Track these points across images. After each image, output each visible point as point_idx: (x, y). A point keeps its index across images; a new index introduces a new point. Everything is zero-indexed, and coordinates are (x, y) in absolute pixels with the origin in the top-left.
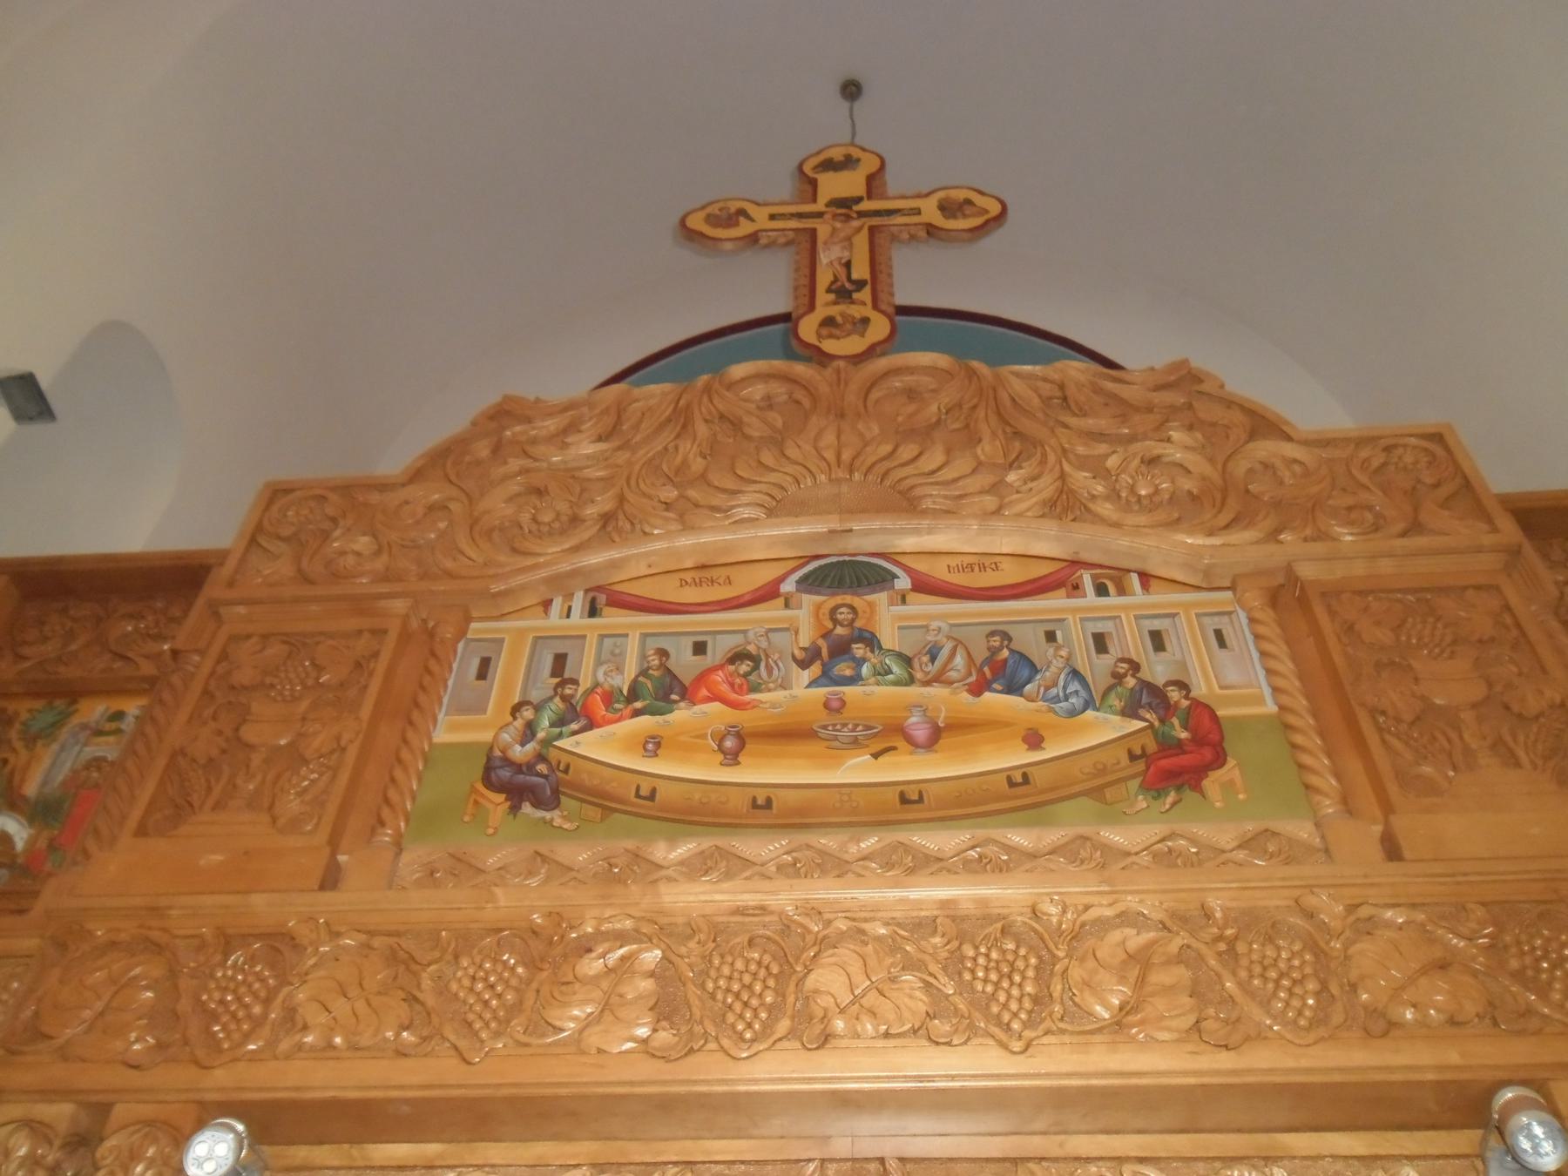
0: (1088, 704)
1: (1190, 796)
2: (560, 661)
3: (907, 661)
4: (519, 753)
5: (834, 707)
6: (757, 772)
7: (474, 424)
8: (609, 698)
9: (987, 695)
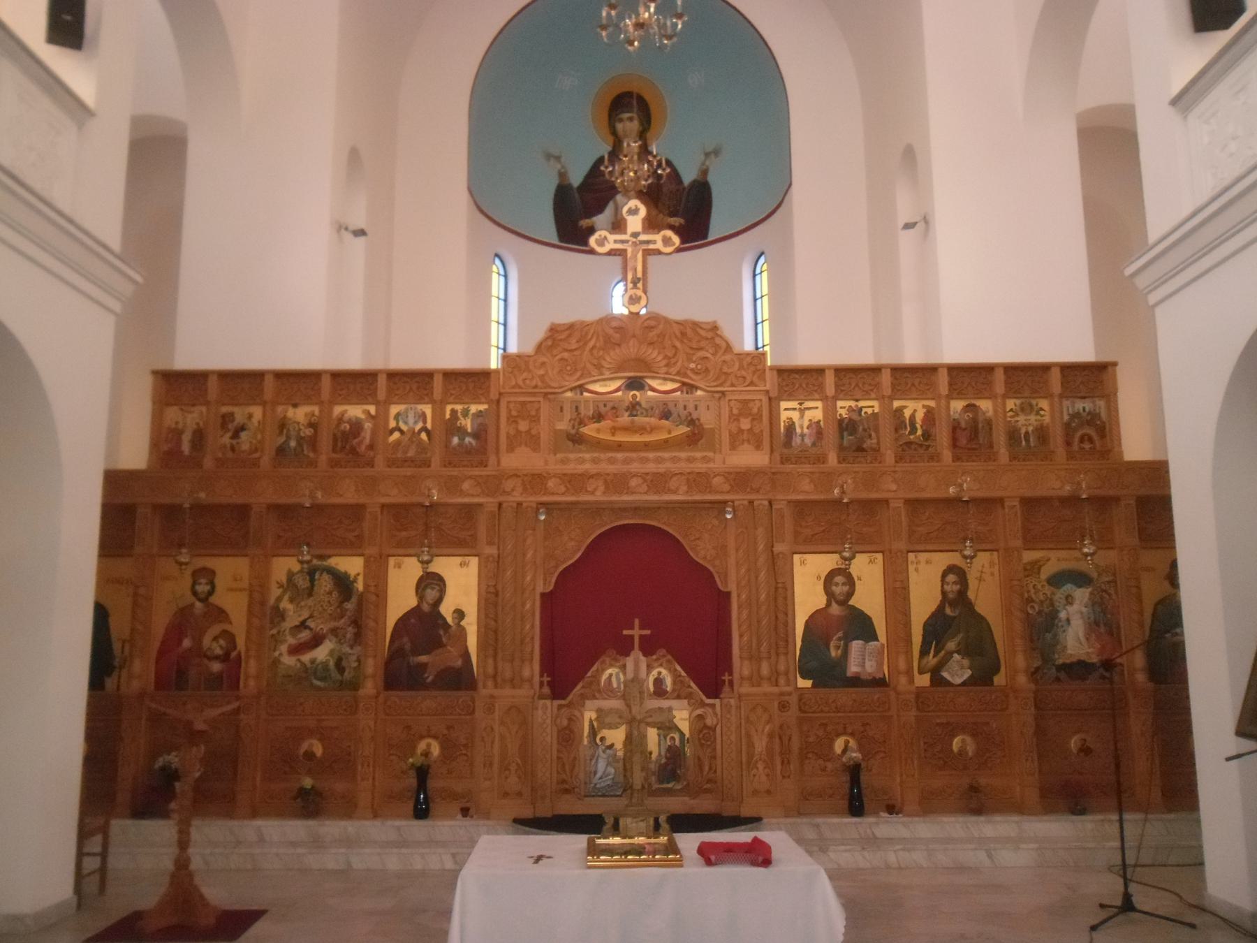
0: (680, 424)
2: (577, 407)
4: (573, 432)
5: (633, 422)
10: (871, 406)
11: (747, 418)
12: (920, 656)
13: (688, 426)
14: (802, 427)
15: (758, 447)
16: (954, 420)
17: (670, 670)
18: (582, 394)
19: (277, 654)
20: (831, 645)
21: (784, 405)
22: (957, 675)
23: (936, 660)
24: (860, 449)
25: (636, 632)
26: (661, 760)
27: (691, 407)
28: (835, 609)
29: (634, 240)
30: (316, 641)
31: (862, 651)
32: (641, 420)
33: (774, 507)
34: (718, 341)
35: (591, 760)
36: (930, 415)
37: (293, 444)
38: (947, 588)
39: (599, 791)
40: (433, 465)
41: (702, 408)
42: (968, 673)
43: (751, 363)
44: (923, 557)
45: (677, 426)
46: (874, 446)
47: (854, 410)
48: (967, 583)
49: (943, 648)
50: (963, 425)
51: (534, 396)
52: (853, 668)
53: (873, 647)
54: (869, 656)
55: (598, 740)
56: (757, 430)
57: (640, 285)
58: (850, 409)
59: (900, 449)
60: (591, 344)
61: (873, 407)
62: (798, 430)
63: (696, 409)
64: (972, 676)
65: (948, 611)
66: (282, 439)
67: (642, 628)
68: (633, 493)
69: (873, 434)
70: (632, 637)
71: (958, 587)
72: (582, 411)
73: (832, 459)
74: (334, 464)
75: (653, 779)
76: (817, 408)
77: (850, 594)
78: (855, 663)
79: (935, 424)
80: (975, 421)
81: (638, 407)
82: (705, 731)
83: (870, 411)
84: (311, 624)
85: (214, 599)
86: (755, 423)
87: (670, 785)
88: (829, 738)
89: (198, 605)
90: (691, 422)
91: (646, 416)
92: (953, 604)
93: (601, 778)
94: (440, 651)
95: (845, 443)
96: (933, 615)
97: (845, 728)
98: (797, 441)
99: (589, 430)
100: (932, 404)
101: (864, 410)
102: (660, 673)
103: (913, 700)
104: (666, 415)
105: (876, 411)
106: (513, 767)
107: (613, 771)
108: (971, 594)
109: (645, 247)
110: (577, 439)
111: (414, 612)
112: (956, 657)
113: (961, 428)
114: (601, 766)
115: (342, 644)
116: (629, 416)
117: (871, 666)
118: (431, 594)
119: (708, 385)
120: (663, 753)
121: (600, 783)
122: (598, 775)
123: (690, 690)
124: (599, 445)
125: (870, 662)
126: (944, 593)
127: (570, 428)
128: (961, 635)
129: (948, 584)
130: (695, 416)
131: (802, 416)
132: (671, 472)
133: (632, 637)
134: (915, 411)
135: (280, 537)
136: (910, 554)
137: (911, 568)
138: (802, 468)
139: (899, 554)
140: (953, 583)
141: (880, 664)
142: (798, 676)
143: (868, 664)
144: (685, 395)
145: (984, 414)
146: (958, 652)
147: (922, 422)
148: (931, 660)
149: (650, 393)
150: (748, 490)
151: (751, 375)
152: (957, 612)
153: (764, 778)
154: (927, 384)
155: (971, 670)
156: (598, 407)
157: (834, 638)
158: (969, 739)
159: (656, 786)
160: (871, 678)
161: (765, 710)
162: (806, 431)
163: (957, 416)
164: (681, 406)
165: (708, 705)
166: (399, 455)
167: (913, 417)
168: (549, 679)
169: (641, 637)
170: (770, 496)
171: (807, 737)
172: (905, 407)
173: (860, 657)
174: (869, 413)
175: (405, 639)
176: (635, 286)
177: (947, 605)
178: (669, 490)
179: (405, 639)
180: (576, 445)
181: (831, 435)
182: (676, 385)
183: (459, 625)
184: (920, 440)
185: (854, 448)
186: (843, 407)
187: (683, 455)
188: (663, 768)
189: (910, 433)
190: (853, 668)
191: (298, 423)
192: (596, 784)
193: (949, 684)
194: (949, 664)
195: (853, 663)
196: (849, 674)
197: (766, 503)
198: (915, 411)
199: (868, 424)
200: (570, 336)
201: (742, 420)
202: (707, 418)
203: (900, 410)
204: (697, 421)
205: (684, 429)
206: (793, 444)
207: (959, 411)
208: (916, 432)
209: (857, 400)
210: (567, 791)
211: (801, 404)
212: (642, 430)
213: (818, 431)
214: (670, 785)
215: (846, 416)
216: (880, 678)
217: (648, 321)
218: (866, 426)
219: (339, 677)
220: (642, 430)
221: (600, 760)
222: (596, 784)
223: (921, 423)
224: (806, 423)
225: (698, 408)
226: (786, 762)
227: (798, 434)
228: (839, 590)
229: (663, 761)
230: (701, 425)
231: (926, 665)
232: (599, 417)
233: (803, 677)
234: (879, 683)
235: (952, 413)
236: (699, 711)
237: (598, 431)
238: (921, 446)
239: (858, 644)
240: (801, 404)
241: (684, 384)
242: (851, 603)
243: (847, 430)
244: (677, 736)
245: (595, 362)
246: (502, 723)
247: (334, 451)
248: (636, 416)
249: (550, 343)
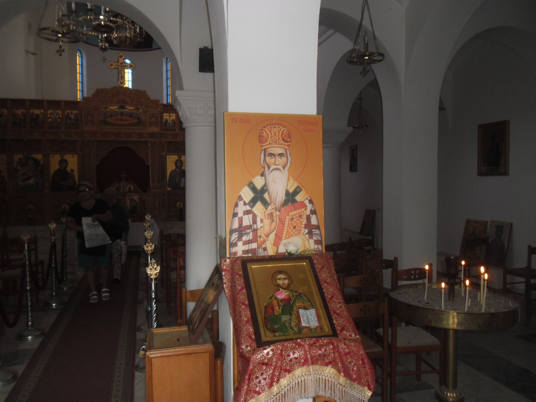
6: (118, 122)
28: (178, 170)
62: (168, 122)
77: (182, 166)
99: (109, 120)
111: (59, 170)
205: (136, 121)
224: (171, 120)
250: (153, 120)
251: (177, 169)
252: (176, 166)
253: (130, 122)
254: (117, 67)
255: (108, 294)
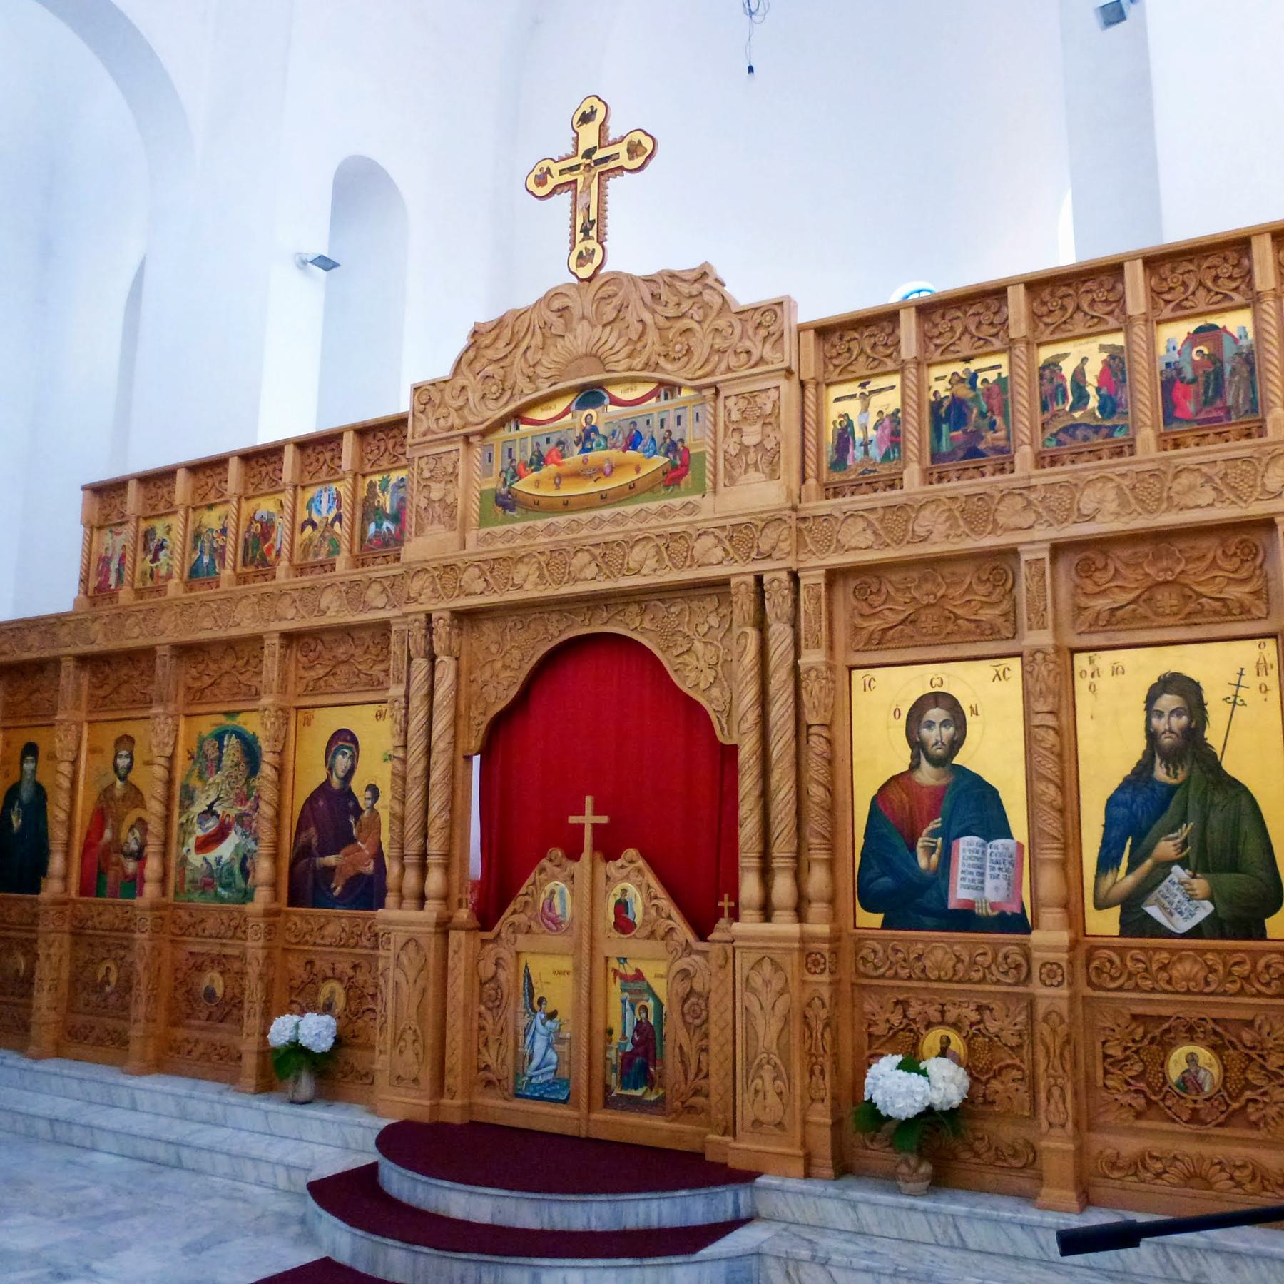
0: (655, 453)
1: (676, 490)
2: (510, 450)
3: (606, 438)
4: (504, 491)
5: (585, 461)
6: (571, 490)
7: (660, 274)
8: (525, 465)
9: (628, 452)
10: (992, 366)
11: (755, 423)
12: (1098, 869)
13: (666, 455)
14: (865, 428)
15: (773, 474)
16: (1168, 365)
17: (639, 887)
18: (517, 428)
19: (185, 850)
20: (920, 844)
21: (836, 391)
22: (1181, 913)
23: (1131, 880)
24: (973, 453)
25: (588, 819)
26: (625, 1045)
27: (671, 423)
28: (928, 775)
29: (588, 161)
30: (219, 836)
31: (978, 859)
32: (596, 456)
33: (802, 582)
34: (708, 296)
35: (525, 1035)
36: (1116, 367)
37: (206, 559)
38: (1160, 724)
39: (535, 1091)
40: (338, 567)
41: (688, 416)
42: (1206, 909)
43: (760, 324)
44: (1105, 660)
45: (649, 457)
46: (1002, 443)
47: (962, 380)
48: (1205, 711)
49: (1148, 853)
50: (1188, 373)
51: (451, 443)
52: (960, 893)
53: (1001, 849)
54: (993, 869)
55: (535, 1004)
56: (770, 444)
57: (593, 233)
58: (956, 379)
59: (1054, 443)
60: (524, 345)
61: (999, 366)
62: (859, 435)
63: (679, 423)
64: (1212, 917)
65: (1160, 773)
66: (196, 556)
67: (597, 812)
68: (576, 580)
69: (998, 420)
70: (581, 827)
71: (1184, 719)
72: (517, 455)
73: (912, 476)
74: (242, 579)
75: (613, 1079)
76: (893, 387)
77: (956, 744)
78: (966, 883)
79: (1124, 381)
80: (1215, 359)
81: (593, 436)
82: (693, 1000)
83: (992, 376)
84: (218, 809)
85: (132, 777)
86: (769, 429)
87: (639, 1092)
88: (911, 1031)
89: (119, 783)
90: (672, 447)
91: (606, 448)
92: (1173, 758)
93: (538, 1068)
94: (350, 848)
95: (945, 446)
96: (1128, 783)
97: (943, 1012)
98: (856, 453)
99: (524, 486)
100: (1118, 340)
101: (981, 376)
102: (624, 891)
103: (1064, 964)
104: (633, 442)
105: (1003, 375)
106: (409, 1037)
107: (555, 1058)
108: (1213, 736)
109: (601, 168)
110: (507, 502)
111: (325, 788)
112: (1178, 872)
113: (1182, 380)
114: (540, 1045)
115: (247, 837)
116: (581, 452)
117: (996, 889)
118: (342, 762)
119: (690, 376)
120: (629, 1034)
121: (537, 1076)
122: (535, 1063)
123: (670, 922)
124: (537, 506)
125: (995, 881)
126: (1152, 736)
127: (500, 485)
128: (1184, 831)
129: (1160, 714)
130: (675, 437)
131: (865, 409)
132: (631, 537)
133: (581, 827)
134: (1084, 360)
135: (189, 688)
136: (1077, 657)
137: (1081, 685)
138: (869, 500)
139: (1039, 656)
140: (1172, 712)
141: (1015, 885)
142: (858, 906)
143: (989, 884)
144: (663, 402)
145: (1236, 341)
146: (1184, 863)
147: (1099, 382)
148: (1123, 879)
149: (611, 408)
150: (753, 555)
151: (760, 346)
152: (1182, 775)
153: (772, 1099)
154: (1106, 301)
155: (1213, 902)
156: (538, 444)
157: (925, 832)
158: (1205, 1055)
159: (617, 1091)
160: (995, 913)
161: (777, 967)
162: (872, 433)
163: (1174, 357)
164: (655, 422)
165: (698, 952)
166: (310, 559)
167: (1079, 374)
168: (720, 904)
169: (596, 827)
170: (790, 563)
171: (870, 1026)
172: (1066, 355)
173: (974, 871)
174: (991, 381)
175: (312, 830)
176: (587, 235)
177: (1158, 761)
178: (629, 569)
179: (312, 830)
180: (508, 512)
181: (916, 436)
182: (649, 388)
183: (372, 808)
184: (1095, 417)
185: (961, 454)
186: (940, 381)
187: (654, 506)
188: (627, 1059)
189: (1073, 408)
190: (960, 893)
191: (212, 530)
192: (531, 1078)
193: (1158, 930)
194: (1162, 887)
195: (959, 882)
196: (952, 905)
197: (784, 576)
198: (1084, 360)
199: (987, 403)
200: (496, 339)
201: (747, 429)
202: (694, 436)
203: (1052, 365)
204: (679, 445)
205: (660, 461)
206: (849, 462)
207: (1178, 347)
208: (1087, 403)
209: (967, 360)
210: (489, 1083)
211: (863, 385)
212: (599, 472)
213: (894, 428)
214: (639, 1092)
215: (948, 393)
216: (1014, 914)
217: (604, 289)
218: (985, 408)
219: (243, 885)
220: (599, 472)
221: (538, 1036)
222: (531, 1078)
223: (1096, 384)
224: (873, 419)
225: (682, 421)
226: (817, 1072)
227: (858, 444)
228: (934, 736)
229: (629, 1048)
230: (686, 450)
231: (1110, 889)
232: (539, 461)
233: (869, 908)
234: (1016, 923)
235: (1162, 351)
236: (684, 962)
237: (537, 484)
238: (1097, 429)
239: (969, 844)
240: (863, 385)
241: (661, 383)
242: (957, 761)
243: (947, 420)
244: (651, 1004)
245: (530, 371)
246: (398, 963)
247: (245, 564)
248: (591, 450)
249: (471, 354)
250: (752, 435)
251: (925, 764)
252: (917, 745)
253: (629, 477)
254: (567, 177)
255: (100, 977)
